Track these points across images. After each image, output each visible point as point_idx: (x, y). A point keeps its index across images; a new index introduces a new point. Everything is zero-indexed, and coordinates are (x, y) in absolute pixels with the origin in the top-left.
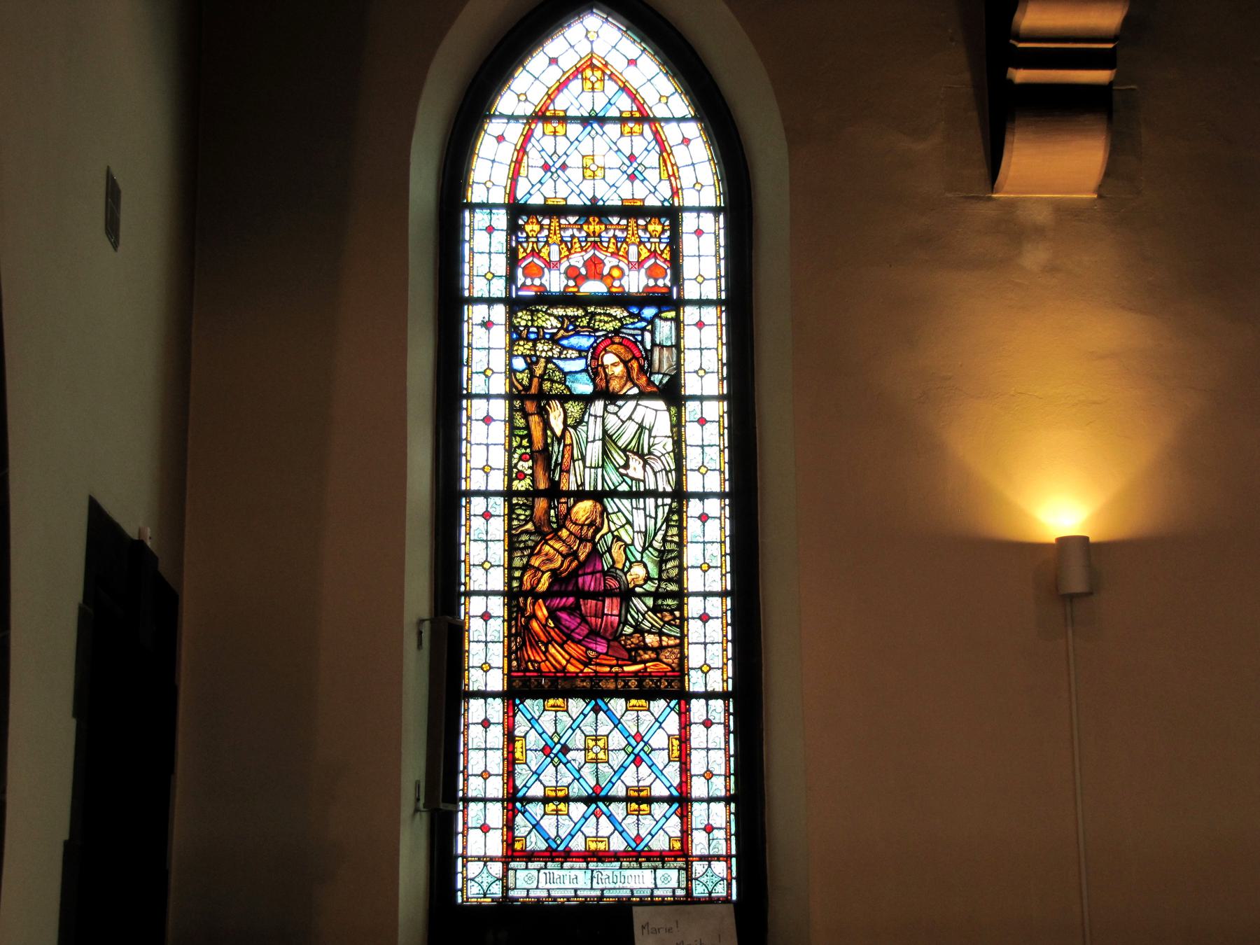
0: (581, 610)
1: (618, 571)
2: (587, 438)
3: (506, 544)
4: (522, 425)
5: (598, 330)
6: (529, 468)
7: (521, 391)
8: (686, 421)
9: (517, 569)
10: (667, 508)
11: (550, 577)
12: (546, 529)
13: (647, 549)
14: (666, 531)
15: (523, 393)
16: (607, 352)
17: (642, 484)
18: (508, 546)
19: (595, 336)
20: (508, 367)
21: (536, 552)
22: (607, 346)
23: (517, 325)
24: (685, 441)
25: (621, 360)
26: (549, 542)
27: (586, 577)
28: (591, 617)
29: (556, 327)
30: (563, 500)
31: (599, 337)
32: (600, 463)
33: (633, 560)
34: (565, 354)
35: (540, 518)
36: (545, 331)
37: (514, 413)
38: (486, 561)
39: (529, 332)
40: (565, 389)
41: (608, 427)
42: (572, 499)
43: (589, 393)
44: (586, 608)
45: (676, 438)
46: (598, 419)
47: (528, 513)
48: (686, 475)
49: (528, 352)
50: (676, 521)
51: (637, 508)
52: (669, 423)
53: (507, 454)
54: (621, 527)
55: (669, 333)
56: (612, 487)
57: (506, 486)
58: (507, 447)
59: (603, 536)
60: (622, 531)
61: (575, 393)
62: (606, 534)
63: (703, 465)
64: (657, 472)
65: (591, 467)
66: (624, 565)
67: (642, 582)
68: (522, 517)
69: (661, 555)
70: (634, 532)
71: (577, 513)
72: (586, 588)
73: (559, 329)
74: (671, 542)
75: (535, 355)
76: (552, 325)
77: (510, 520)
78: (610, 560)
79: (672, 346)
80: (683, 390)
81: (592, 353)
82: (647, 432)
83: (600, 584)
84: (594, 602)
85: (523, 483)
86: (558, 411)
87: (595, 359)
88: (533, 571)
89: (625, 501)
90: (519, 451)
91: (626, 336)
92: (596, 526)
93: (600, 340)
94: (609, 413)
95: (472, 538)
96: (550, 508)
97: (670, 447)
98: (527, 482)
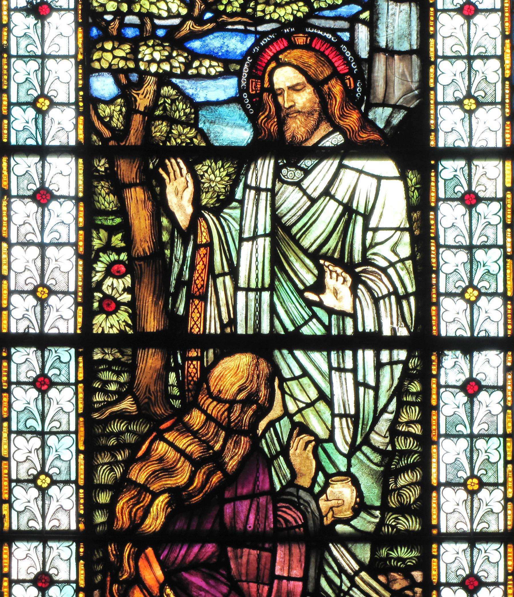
0: (228, 568)
1: (302, 493)
2: (241, 232)
3: (82, 439)
4: (111, 207)
5: (262, 21)
6: (125, 290)
7: (109, 139)
8: (438, 199)
9: (104, 488)
10: (398, 369)
11: (169, 504)
12: (159, 410)
13: (359, 448)
14: (398, 413)
15: (112, 143)
16: (280, 64)
17: (349, 322)
18: (85, 443)
19: (256, 32)
20: (81, 93)
21: (140, 454)
22: (282, 52)
23: (100, 10)
24: (436, 238)
25: (310, 80)
26: (166, 436)
27: (238, 503)
28: (248, 582)
29: (178, 15)
30: (193, 354)
31: (265, 34)
32: (267, 281)
33: (331, 470)
34: (197, 68)
35: (148, 387)
36: (157, 22)
37: (95, 183)
38: (42, 472)
39: (123, 25)
40: (195, 137)
41: (283, 209)
42: (211, 351)
43: (244, 144)
44: (238, 565)
45: (417, 232)
46: (263, 195)
47: (124, 378)
48: (437, 304)
49: (122, 64)
50: (417, 394)
51: (341, 370)
52: (404, 203)
53: (81, 262)
54: (308, 405)
55: (405, 25)
56: (291, 328)
57: (79, 326)
58: (81, 249)
59: (272, 424)
60: (309, 413)
61: (217, 144)
62: (279, 419)
63: (471, 285)
64: (379, 299)
65: (248, 289)
66: (314, 480)
67: (349, 514)
68: (113, 387)
69: (387, 460)
70: (333, 415)
71: (221, 378)
72: (240, 526)
73: (185, 19)
74: (407, 435)
75: (137, 70)
76: (169, 10)
77: (89, 392)
78: (288, 472)
79: (410, 52)
80: (432, 137)
81: (252, 67)
82: (360, 220)
83: (266, 517)
84: (254, 553)
85: (113, 319)
86: (183, 179)
87: (256, 77)
88: (134, 492)
89: (317, 356)
90: (104, 258)
91: (319, 32)
92: (259, 406)
93: (267, 39)
94: (284, 182)
95: (14, 428)
96: (167, 368)
97: (405, 251)
98: (123, 315)
